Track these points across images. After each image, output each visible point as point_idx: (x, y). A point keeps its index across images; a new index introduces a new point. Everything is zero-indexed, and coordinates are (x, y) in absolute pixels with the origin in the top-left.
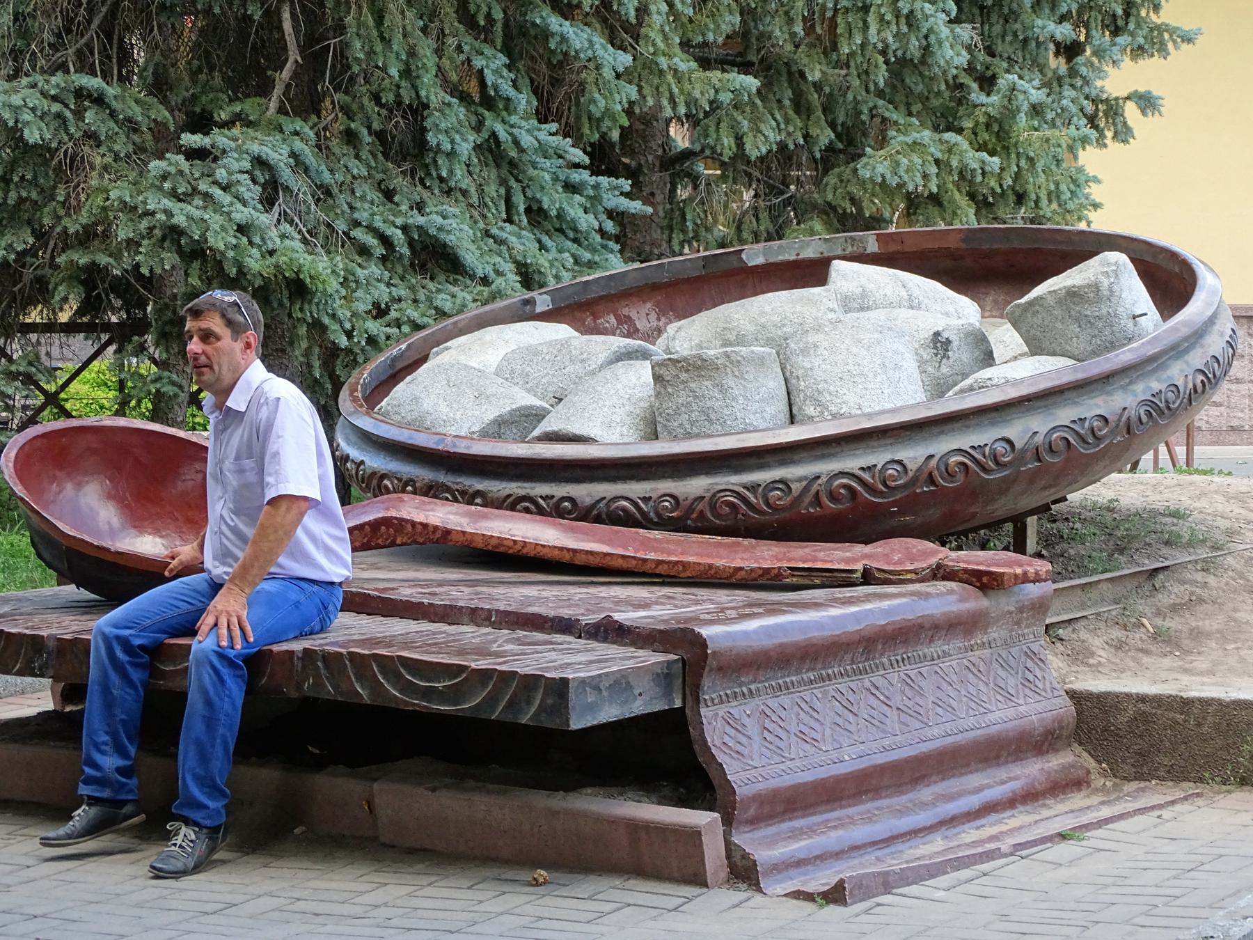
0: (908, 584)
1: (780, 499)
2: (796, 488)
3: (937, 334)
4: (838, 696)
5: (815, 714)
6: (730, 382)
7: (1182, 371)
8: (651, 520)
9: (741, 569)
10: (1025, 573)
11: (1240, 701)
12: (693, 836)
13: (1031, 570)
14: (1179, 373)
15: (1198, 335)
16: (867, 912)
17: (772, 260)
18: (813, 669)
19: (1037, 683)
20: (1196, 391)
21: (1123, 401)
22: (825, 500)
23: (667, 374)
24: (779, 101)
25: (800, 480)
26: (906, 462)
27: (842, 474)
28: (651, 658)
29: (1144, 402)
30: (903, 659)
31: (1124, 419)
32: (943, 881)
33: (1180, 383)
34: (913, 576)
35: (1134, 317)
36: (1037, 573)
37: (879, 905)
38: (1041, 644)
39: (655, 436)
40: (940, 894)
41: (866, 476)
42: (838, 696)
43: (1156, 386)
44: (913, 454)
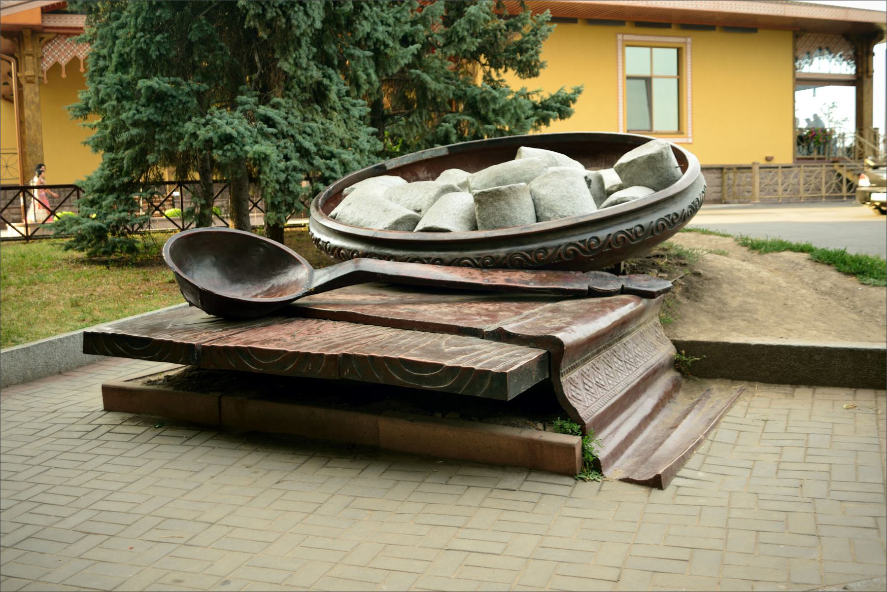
2: (550, 252)
6: (513, 201)
12: (571, 448)
22: (563, 256)
23: (483, 199)
28: (533, 354)
39: (475, 228)
41: (582, 245)
44: (602, 234)
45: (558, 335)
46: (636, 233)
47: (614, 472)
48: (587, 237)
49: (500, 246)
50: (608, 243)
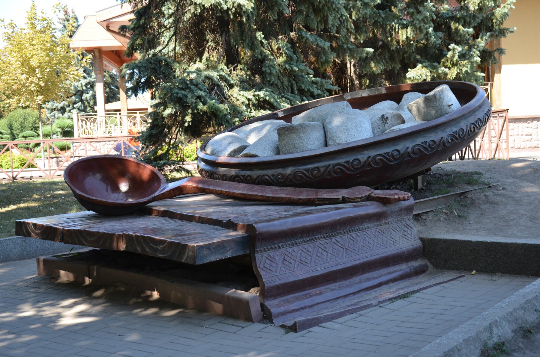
0: (357, 202)
1: (317, 174)
2: (322, 170)
3: (383, 116)
4: (320, 246)
5: (309, 253)
7: (465, 124)
8: (275, 182)
9: (301, 199)
10: (399, 198)
11: (479, 242)
13: (401, 197)
14: (464, 125)
15: (474, 111)
16: (302, 336)
17: (354, 97)
18: (309, 236)
19: (408, 235)
20: (471, 131)
21: (444, 135)
24: (385, 57)
25: (323, 167)
26: (360, 159)
27: (338, 164)
29: (450, 135)
30: (350, 231)
31: (442, 141)
32: (340, 320)
33: (465, 129)
34: (359, 200)
35: (449, 106)
36: (404, 197)
37: (310, 332)
38: (411, 222)
39: (278, 152)
40: (337, 326)
41: (346, 165)
42: (320, 246)
43: (454, 129)
45: (254, 225)
46: (393, 155)
47: (278, 321)
48: (351, 159)
49: (288, 166)
50: (367, 163)
